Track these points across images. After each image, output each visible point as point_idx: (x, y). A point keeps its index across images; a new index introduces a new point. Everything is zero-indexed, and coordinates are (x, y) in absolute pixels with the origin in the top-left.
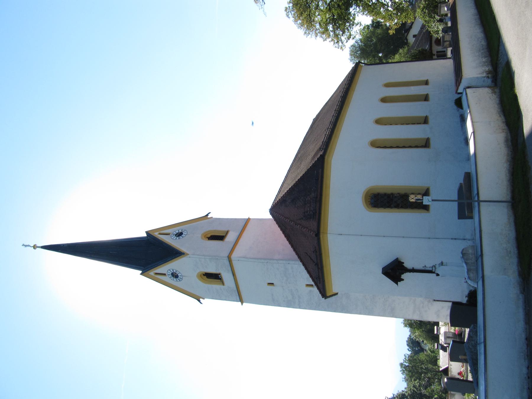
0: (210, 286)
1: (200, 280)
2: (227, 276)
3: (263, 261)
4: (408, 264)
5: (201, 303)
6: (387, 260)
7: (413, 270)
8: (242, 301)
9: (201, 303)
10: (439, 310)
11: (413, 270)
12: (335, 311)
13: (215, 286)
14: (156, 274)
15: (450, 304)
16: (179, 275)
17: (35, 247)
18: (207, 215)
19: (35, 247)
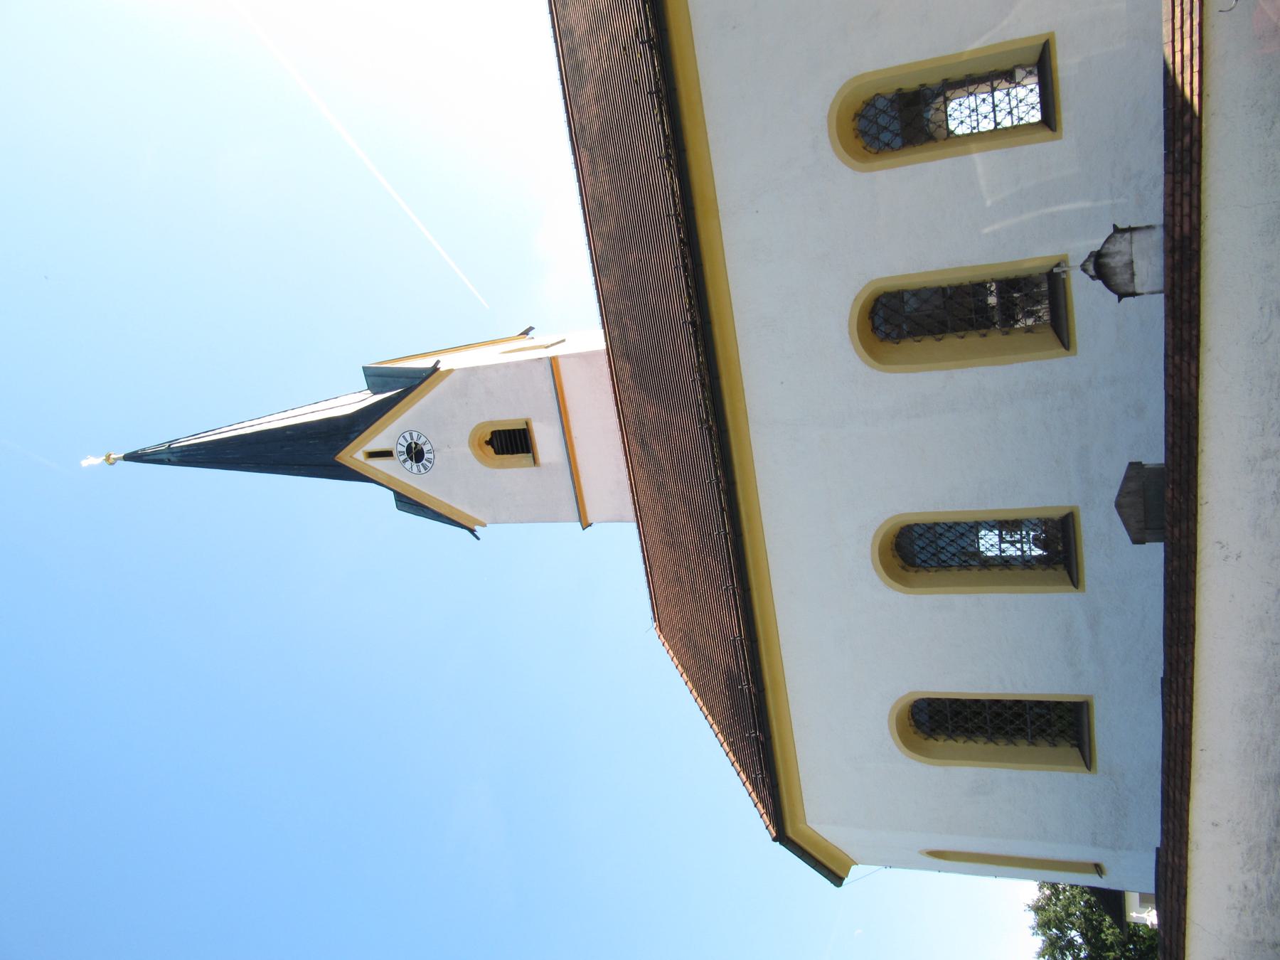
2: (546, 439)
14: (372, 455)
16: (426, 448)
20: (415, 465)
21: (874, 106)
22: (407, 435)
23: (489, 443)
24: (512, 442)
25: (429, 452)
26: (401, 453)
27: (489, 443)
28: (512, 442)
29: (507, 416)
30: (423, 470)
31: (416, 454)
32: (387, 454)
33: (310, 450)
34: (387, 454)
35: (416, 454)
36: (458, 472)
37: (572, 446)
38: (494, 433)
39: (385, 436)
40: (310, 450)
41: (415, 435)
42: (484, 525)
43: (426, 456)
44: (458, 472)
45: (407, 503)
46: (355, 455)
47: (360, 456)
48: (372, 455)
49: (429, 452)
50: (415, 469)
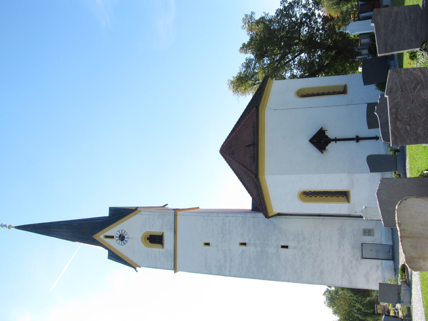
0: (150, 249)
1: (143, 242)
2: (168, 239)
3: (204, 214)
4: (330, 134)
5: (137, 271)
6: (313, 150)
7: (336, 140)
8: (175, 269)
9: (137, 271)
10: (368, 272)
11: (336, 140)
12: (264, 279)
13: (155, 249)
14: (107, 237)
15: (366, 105)
16: (126, 237)
17: (10, 227)
18: (165, 206)
19: (10, 227)
20: (121, 242)
21: (289, 16)
22: (120, 231)
23: (148, 239)
24: (156, 239)
25: (127, 238)
26: (117, 237)
27: (148, 239)
28: (156, 239)
29: (156, 230)
30: (123, 244)
31: (122, 238)
32: (112, 237)
33: (83, 231)
34: (112, 237)
35: (122, 238)
36: (134, 247)
37: (176, 250)
38: (150, 236)
39: (114, 230)
40: (83, 231)
41: (123, 231)
42: (140, 267)
43: (125, 239)
44: (134, 247)
45: (114, 256)
46: (100, 236)
47: (102, 237)
48: (107, 237)
49: (127, 238)
50: (120, 243)
